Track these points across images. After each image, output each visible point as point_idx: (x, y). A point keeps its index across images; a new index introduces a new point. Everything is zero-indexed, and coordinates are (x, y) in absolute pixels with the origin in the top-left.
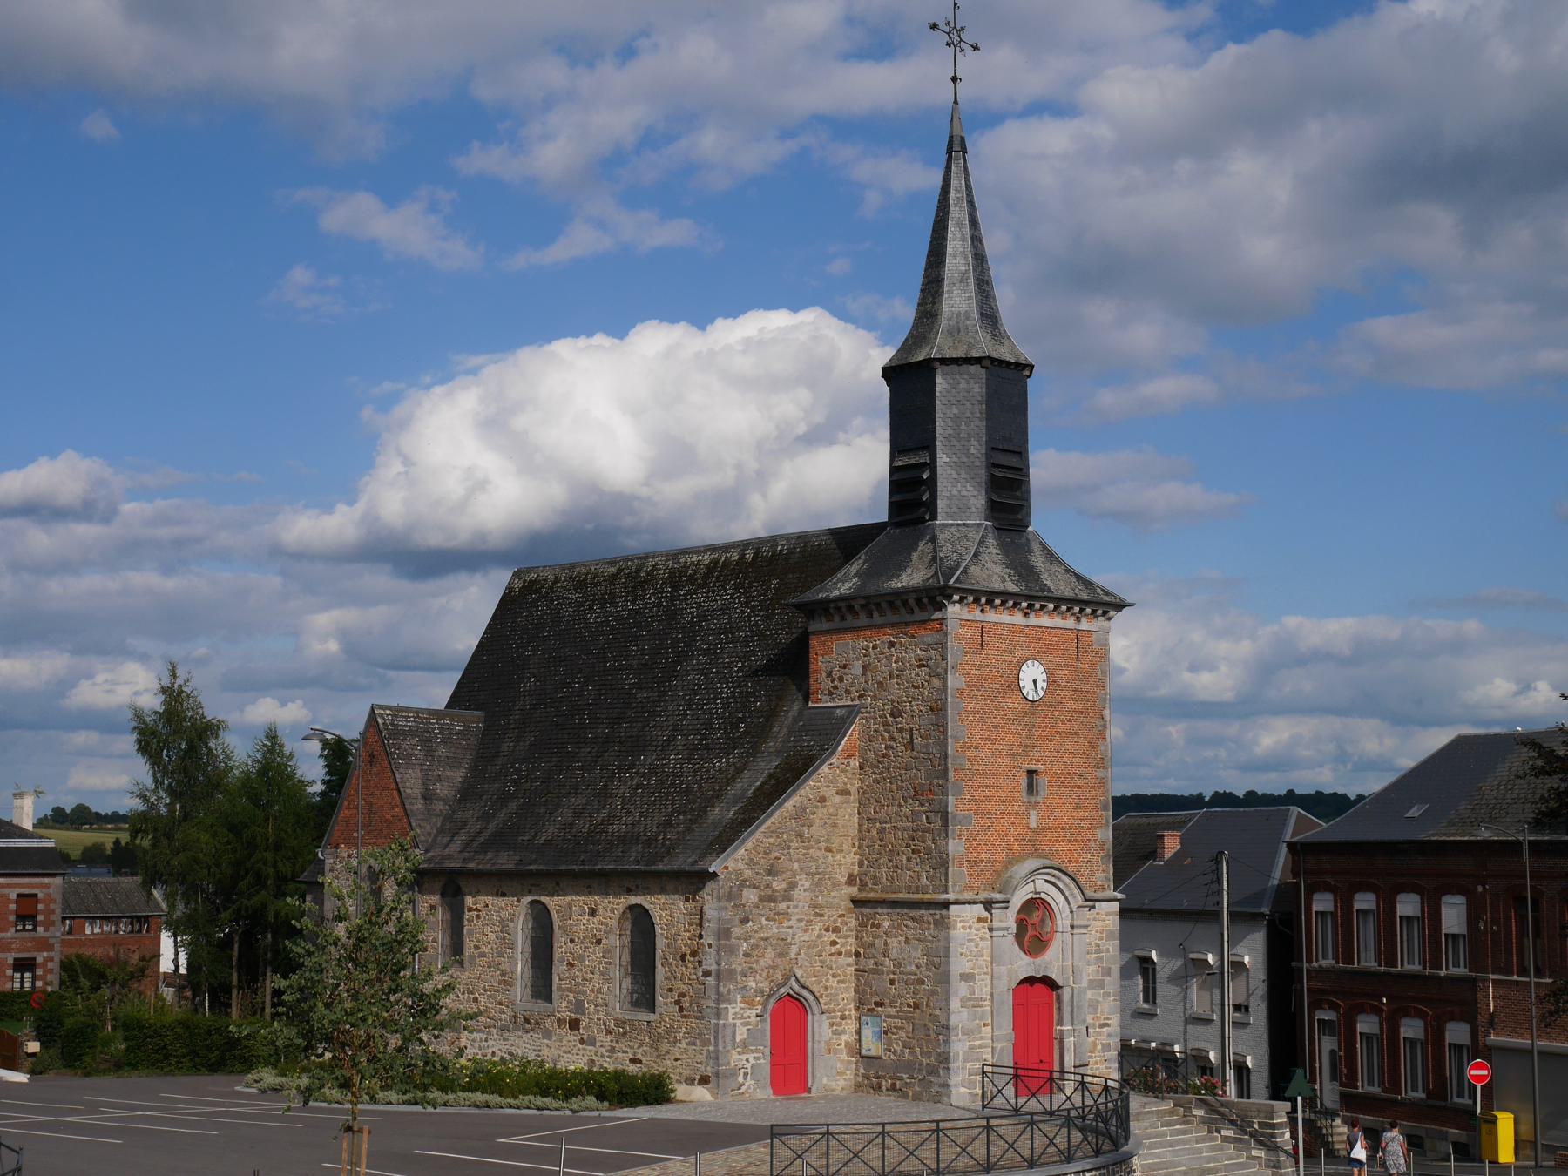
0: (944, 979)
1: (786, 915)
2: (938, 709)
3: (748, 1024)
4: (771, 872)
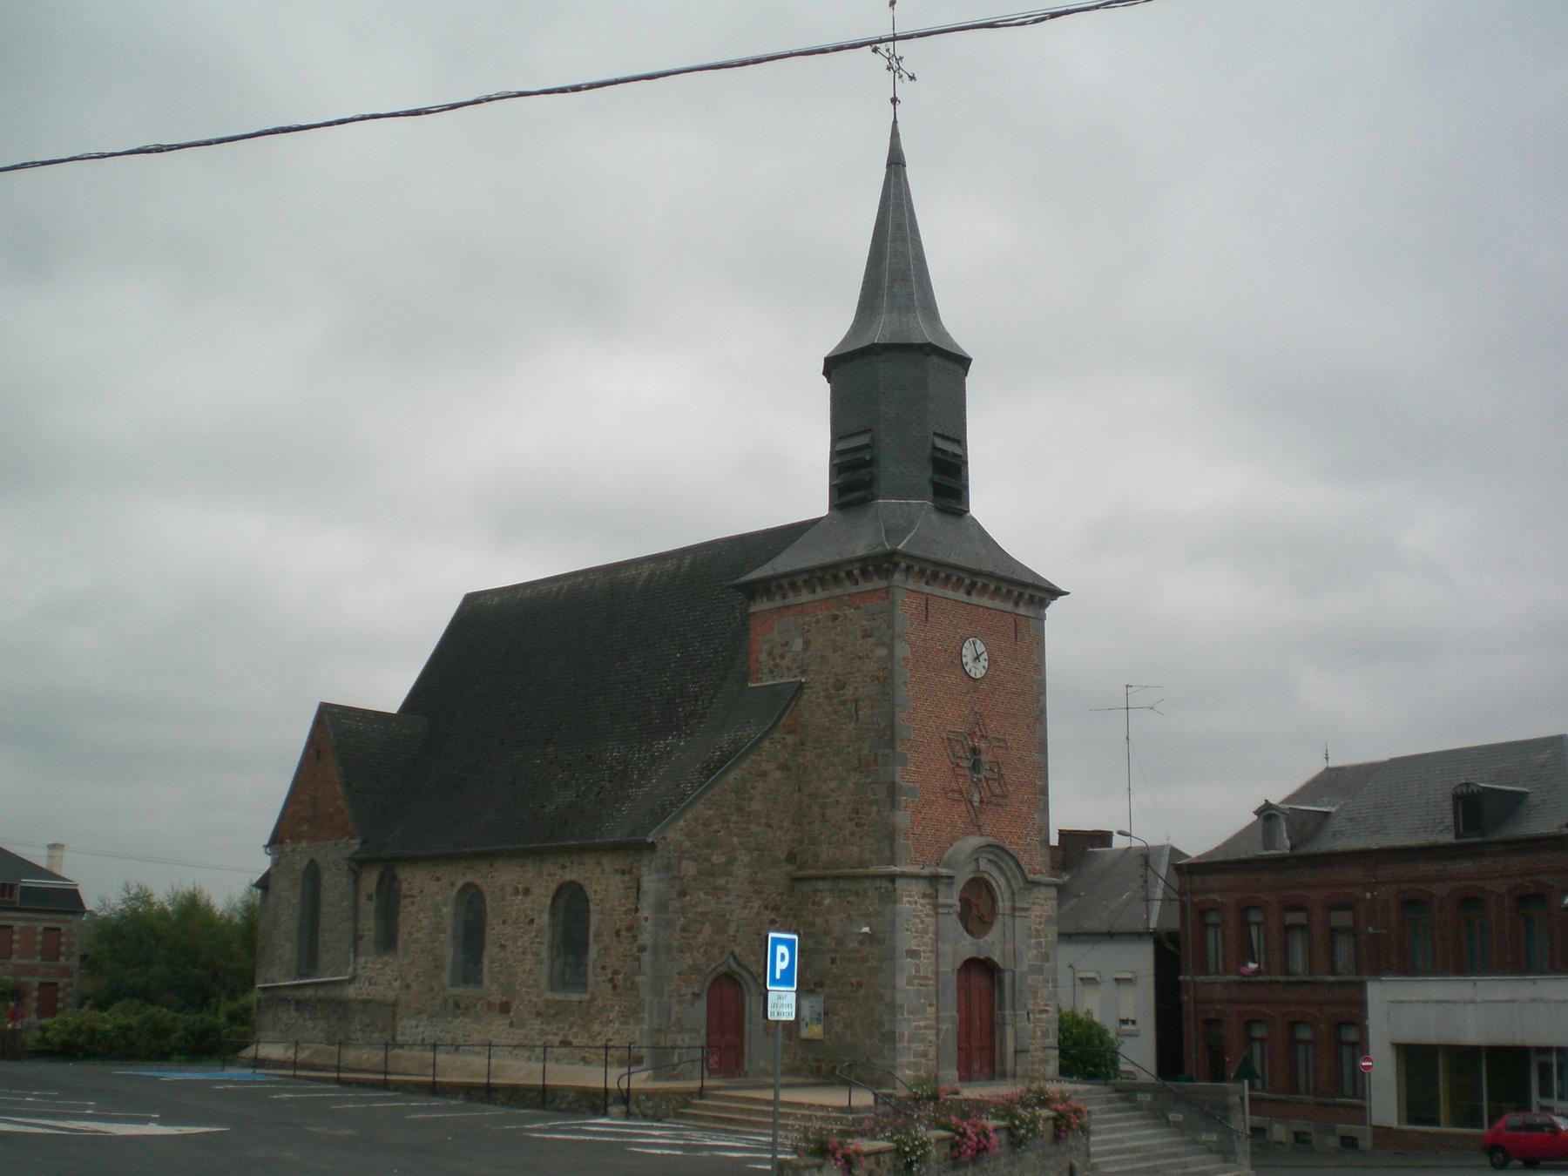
2: (885, 680)
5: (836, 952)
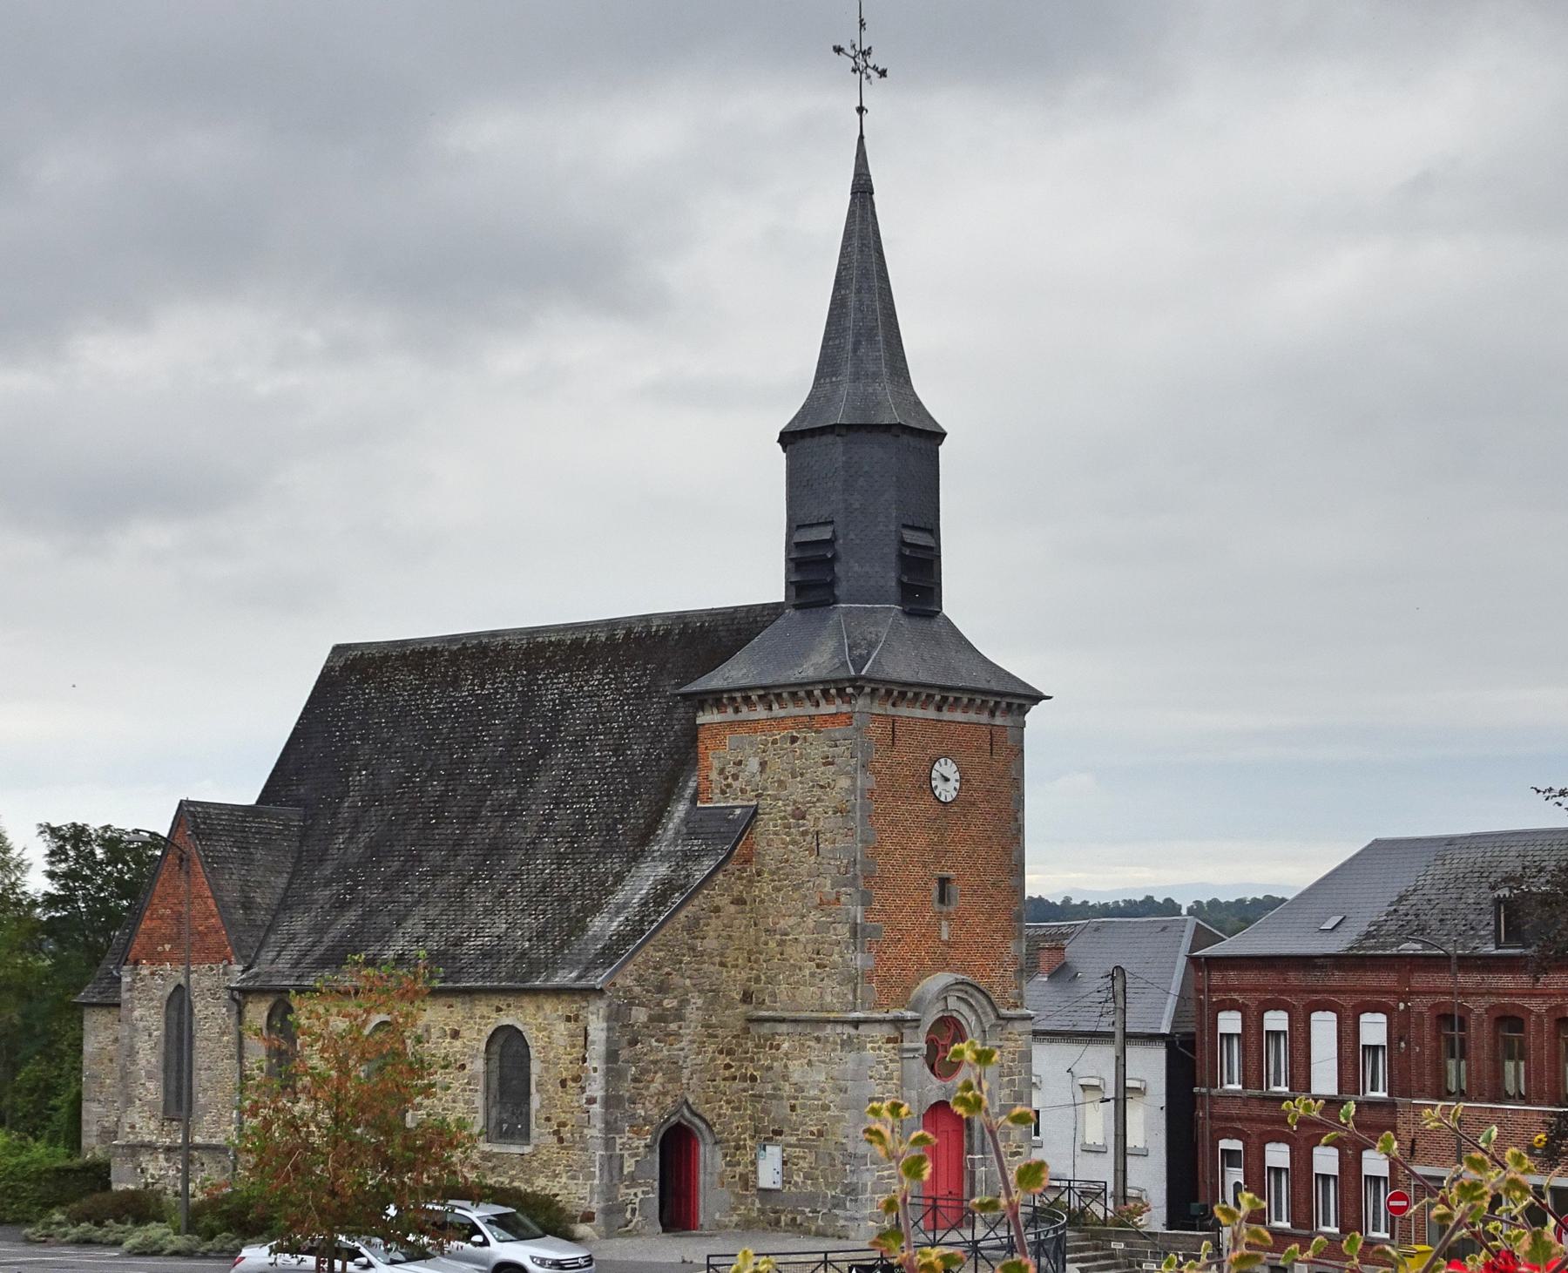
3: (636, 1155)
5: (796, 1098)
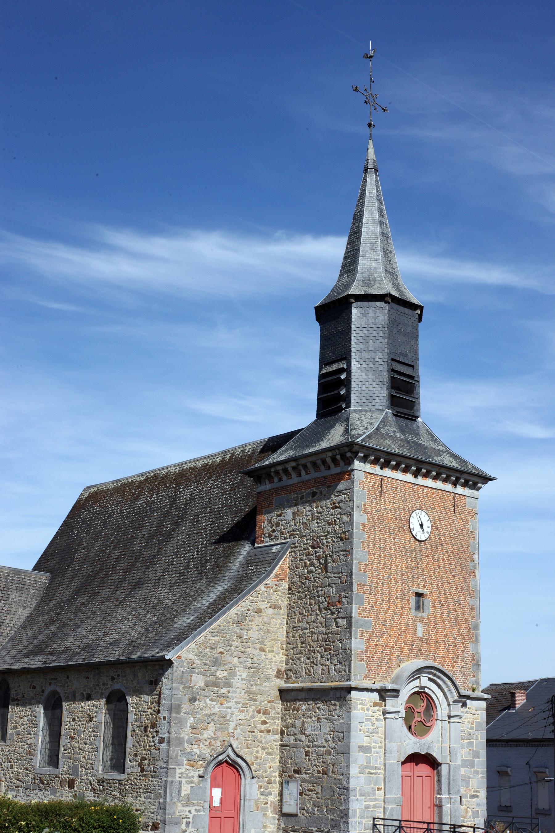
0: (346, 752)
1: (226, 697)
3: (191, 782)
4: (216, 663)
